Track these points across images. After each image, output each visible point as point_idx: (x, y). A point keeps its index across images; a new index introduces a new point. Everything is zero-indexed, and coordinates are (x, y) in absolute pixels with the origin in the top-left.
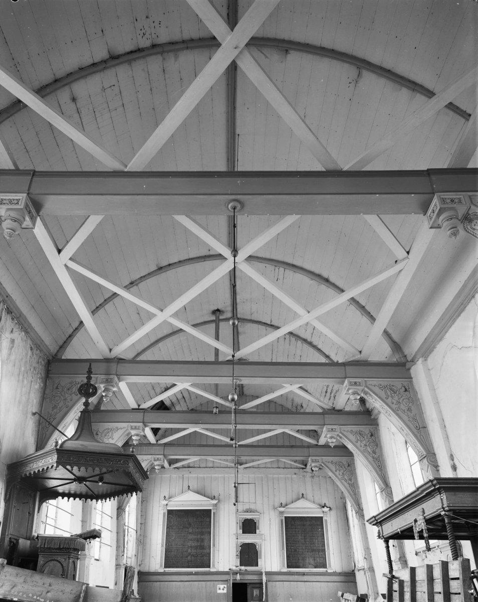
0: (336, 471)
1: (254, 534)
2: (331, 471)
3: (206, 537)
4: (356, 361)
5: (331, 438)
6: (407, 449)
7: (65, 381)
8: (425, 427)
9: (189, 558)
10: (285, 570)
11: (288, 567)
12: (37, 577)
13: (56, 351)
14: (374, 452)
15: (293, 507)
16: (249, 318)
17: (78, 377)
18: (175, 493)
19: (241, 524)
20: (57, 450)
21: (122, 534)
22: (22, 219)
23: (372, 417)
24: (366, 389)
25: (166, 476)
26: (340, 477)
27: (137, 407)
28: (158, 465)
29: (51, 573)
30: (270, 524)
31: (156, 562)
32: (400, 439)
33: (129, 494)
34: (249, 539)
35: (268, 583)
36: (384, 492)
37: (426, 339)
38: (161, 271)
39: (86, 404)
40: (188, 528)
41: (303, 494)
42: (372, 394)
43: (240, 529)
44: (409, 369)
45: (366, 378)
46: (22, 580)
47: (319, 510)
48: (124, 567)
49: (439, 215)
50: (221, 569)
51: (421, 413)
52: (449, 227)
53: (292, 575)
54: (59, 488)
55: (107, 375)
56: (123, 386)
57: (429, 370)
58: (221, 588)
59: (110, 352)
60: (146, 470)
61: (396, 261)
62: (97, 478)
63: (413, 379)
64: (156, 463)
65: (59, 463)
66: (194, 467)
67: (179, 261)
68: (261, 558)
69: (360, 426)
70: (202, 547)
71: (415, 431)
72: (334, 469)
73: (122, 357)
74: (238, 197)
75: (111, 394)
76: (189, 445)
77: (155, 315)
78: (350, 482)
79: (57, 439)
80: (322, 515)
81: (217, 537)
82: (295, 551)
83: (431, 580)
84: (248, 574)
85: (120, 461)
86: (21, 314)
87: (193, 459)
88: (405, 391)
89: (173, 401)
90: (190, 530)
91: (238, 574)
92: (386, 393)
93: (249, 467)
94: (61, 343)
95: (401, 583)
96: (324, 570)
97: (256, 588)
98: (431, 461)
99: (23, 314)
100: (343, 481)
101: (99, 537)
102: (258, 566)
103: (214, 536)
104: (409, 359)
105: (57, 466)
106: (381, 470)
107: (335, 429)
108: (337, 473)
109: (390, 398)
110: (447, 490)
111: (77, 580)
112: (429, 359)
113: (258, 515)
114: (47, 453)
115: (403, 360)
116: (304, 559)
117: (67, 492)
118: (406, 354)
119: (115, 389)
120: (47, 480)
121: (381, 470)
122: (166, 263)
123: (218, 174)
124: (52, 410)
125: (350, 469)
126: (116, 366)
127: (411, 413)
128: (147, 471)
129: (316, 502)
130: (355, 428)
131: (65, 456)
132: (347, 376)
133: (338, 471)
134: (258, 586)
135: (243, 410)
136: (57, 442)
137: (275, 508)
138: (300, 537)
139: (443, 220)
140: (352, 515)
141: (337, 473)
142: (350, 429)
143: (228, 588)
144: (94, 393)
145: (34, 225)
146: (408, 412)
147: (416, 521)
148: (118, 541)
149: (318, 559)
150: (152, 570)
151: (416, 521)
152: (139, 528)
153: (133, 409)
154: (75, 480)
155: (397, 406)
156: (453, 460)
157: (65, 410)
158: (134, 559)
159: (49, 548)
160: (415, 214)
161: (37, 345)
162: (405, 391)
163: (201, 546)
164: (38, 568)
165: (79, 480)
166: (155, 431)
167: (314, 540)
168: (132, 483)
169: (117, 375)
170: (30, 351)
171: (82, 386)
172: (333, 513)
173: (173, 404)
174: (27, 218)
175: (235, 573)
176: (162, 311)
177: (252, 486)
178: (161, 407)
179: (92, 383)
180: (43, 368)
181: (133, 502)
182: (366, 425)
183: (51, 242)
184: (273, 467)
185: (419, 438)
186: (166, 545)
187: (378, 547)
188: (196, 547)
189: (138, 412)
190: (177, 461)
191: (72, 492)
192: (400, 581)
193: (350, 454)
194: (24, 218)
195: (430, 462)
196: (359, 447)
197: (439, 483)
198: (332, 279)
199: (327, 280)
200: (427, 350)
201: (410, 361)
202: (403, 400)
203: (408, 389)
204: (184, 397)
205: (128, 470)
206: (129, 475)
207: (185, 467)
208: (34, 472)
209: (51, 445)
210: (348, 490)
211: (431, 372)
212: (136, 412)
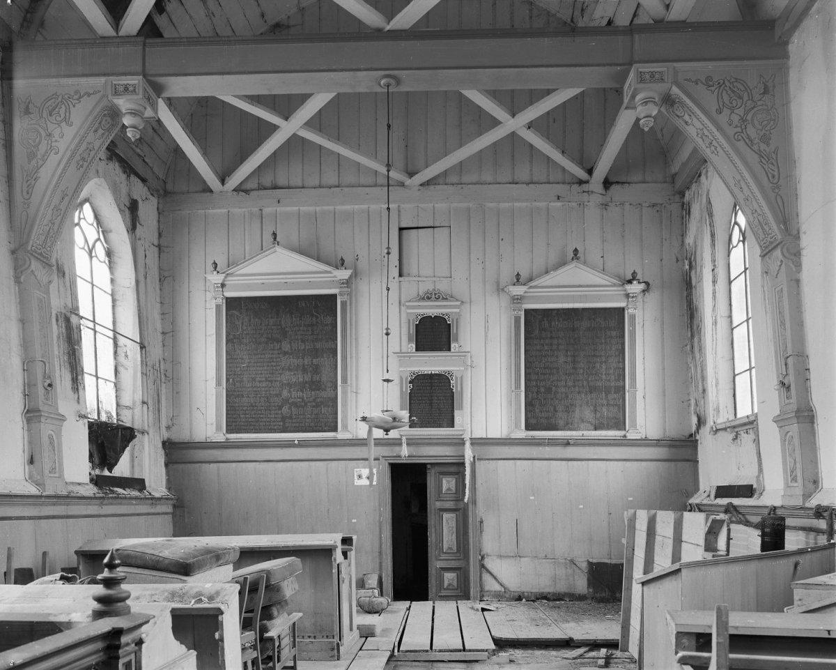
0: (720, 111)
9: (285, 410)
10: (522, 433)
11: (529, 427)
15: (549, 283)
19: (413, 331)
30: (486, 329)
34: (432, 363)
41: (576, 251)
43: (410, 340)
47: (617, 291)
58: (364, 477)
68: (461, 408)
78: (763, 147)
80: (622, 305)
82: (549, 390)
84: (425, 444)
90: (286, 346)
96: (622, 433)
100: (741, 144)
102: (453, 426)
108: (723, 119)
116: (569, 409)
127: (768, 145)
133: (726, 112)
134: (452, 469)
138: (562, 359)
149: (604, 409)
167: (598, 365)
172: (653, 298)
177: (441, 234)
186: (228, 380)
195: (787, 255)
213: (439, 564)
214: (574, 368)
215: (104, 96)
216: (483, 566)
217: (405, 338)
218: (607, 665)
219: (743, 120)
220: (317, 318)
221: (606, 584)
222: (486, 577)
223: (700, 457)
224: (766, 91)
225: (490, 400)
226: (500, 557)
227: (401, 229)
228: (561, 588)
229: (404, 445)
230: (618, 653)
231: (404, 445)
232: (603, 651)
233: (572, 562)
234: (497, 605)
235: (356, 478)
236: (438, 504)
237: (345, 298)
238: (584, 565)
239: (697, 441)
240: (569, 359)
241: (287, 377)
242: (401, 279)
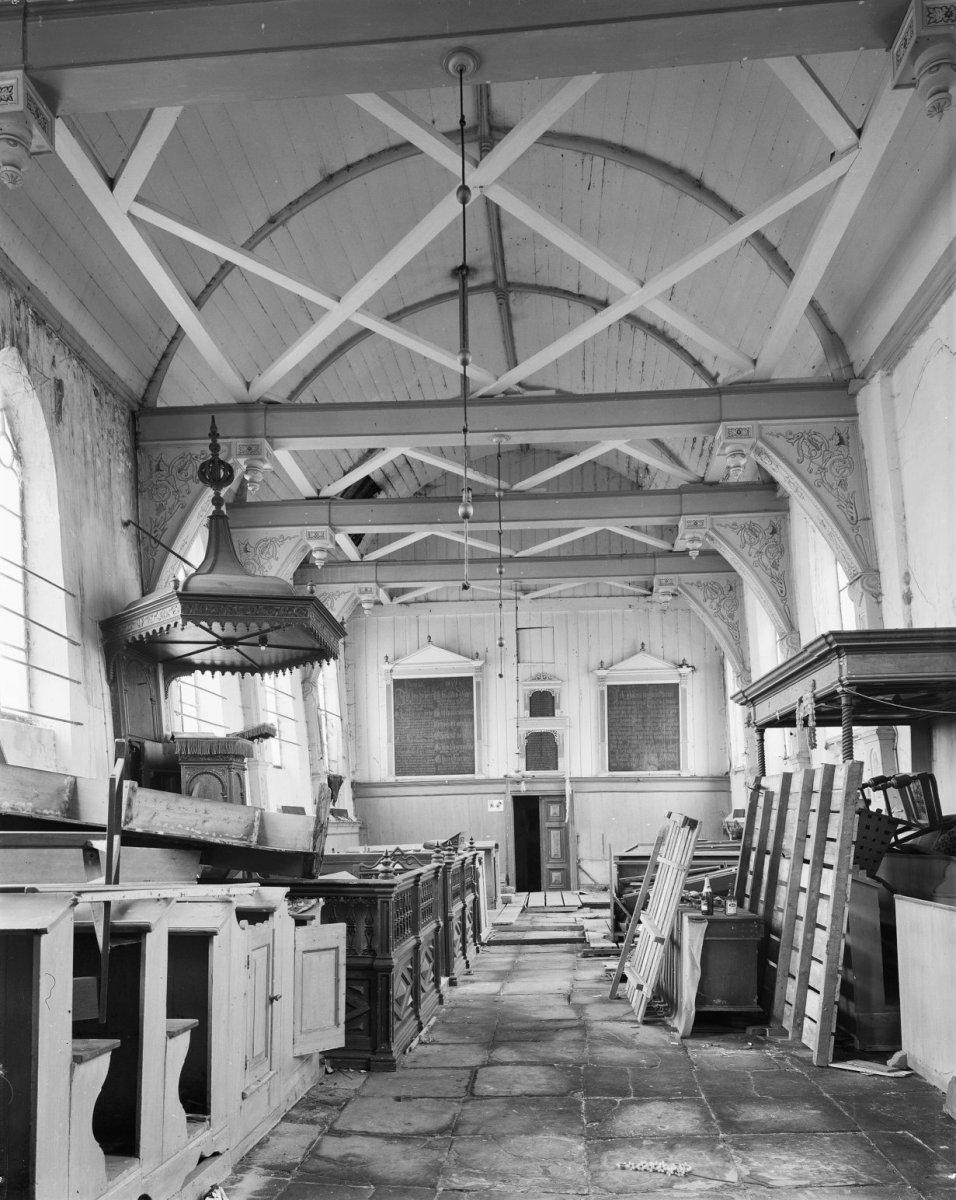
2: (696, 601)
3: (465, 724)
4: (745, 383)
5: (693, 540)
7: (170, 454)
8: (868, 519)
9: (437, 759)
10: (607, 774)
12: (184, 802)
13: (142, 391)
14: (775, 566)
15: (624, 667)
16: (532, 281)
17: (192, 445)
18: (400, 647)
19: (528, 701)
20: (178, 594)
21: (315, 726)
22: (26, 134)
23: (779, 494)
24: (760, 444)
25: (386, 619)
26: (712, 612)
27: (315, 494)
28: (368, 602)
29: (205, 795)
30: (580, 699)
31: (380, 764)
33: (317, 664)
34: (542, 725)
35: (575, 795)
36: (785, 641)
37: (892, 329)
38: (333, 185)
39: (217, 501)
40: (432, 710)
42: (771, 454)
43: (525, 708)
44: (854, 395)
46: (163, 806)
47: (675, 672)
48: (326, 776)
49: (914, 55)
51: (864, 488)
52: (933, 89)
53: (618, 781)
54: (193, 657)
56: (283, 456)
57: (893, 396)
59: (248, 389)
60: (339, 620)
61: (833, 155)
62: (255, 639)
64: (364, 598)
65: (186, 618)
66: (437, 601)
67: (369, 157)
69: (751, 514)
70: (459, 741)
71: (847, 526)
72: (701, 598)
73: (273, 399)
74: (470, 41)
75: (260, 477)
76: (423, 562)
77: (326, 310)
79: (175, 573)
80: (677, 682)
81: (484, 725)
82: (625, 743)
83: (808, 791)
84: (539, 783)
85: (291, 609)
86: (62, 322)
87: (430, 588)
89: (387, 471)
90: (437, 714)
91: (523, 783)
92: (799, 448)
93: (542, 598)
94: (149, 372)
95: (769, 796)
96: (677, 772)
97: (555, 803)
98: (869, 586)
99: (66, 322)
100: (717, 619)
101: (273, 736)
104: (858, 371)
105: (184, 624)
107: (702, 522)
108: (707, 605)
110: (850, 650)
111: (249, 803)
112: (896, 372)
114: (162, 600)
115: (845, 374)
116: (639, 756)
117: (208, 662)
119: (267, 466)
120: (171, 645)
122: (341, 165)
125: (732, 593)
126: (263, 418)
128: (342, 623)
129: (666, 657)
130: (742, 519)
131: (195, 605)
132: (724, 416)
133: (709, 601)
134: (557, 799)
135: (520, 491)
136: (176, 582)
137: (589, 671)
138: (634, 721)
139: (921, 69)
141: (707, 605)
143: (506, 803)
144: (229, 479)
145: (52, 142)
146: (840, 489)
147: (801, 701)
148: (310, 736)
150: (376, 779)
151: (801, 701)
152: (345, 713)
153: (307, 499)
154: (218, 644)
156: (908, 583)
157: (179, 512)
158: (341, 762)
159: (195, 756)
160: (867, 48)
161: (104, 384)
163: (456, 739)
164: (183, 786)
165: (227, 642)
166: (357, 539)
168: (318, 646)
169: (267, 437)
170: (94, 399)
171: (203, 465)
173: (387, 477)
174: (36, 131)
176: (338, 299)
177: (547, 633)
178: (367, 489)
179: (222, 456)
180: (125, 428)
181: (328, 674)
182: (766, 511)
183: (94, 170)
184: (588, 594)
185: (854, 541)
186: (396, 738)
187: (739, 736)
188: (449, 742)
189: (318, 504)
190: (404, 591)
191: (218, 662)
192: (767, 793)
193: (728, 569)
194: (30, 132)
196: (709, 609)
197: (837, 641)
198: (710, 182)
199: (698, 185)
200: (893, 353)
201: (859, 378)
203: (845, 440)
205: (308, 625)
206: (311, 633)
207: (421, 602)
208: (148, 634)
209: (165, 588)
210: (725, 637)
211: (896, 401)
212: (313, 504)
214: (644, 727)
215: (354, 594)
216: (579, 867)
219: (718, 605)
222: (582, 874)
223: (732, 790)
224: (731, 589)
225: (583, 749)
226: (592, 860)
227: (518, 629)
236: (548, 824)
237: (479, 679)
240: (640, 720)
241: (437, 735)
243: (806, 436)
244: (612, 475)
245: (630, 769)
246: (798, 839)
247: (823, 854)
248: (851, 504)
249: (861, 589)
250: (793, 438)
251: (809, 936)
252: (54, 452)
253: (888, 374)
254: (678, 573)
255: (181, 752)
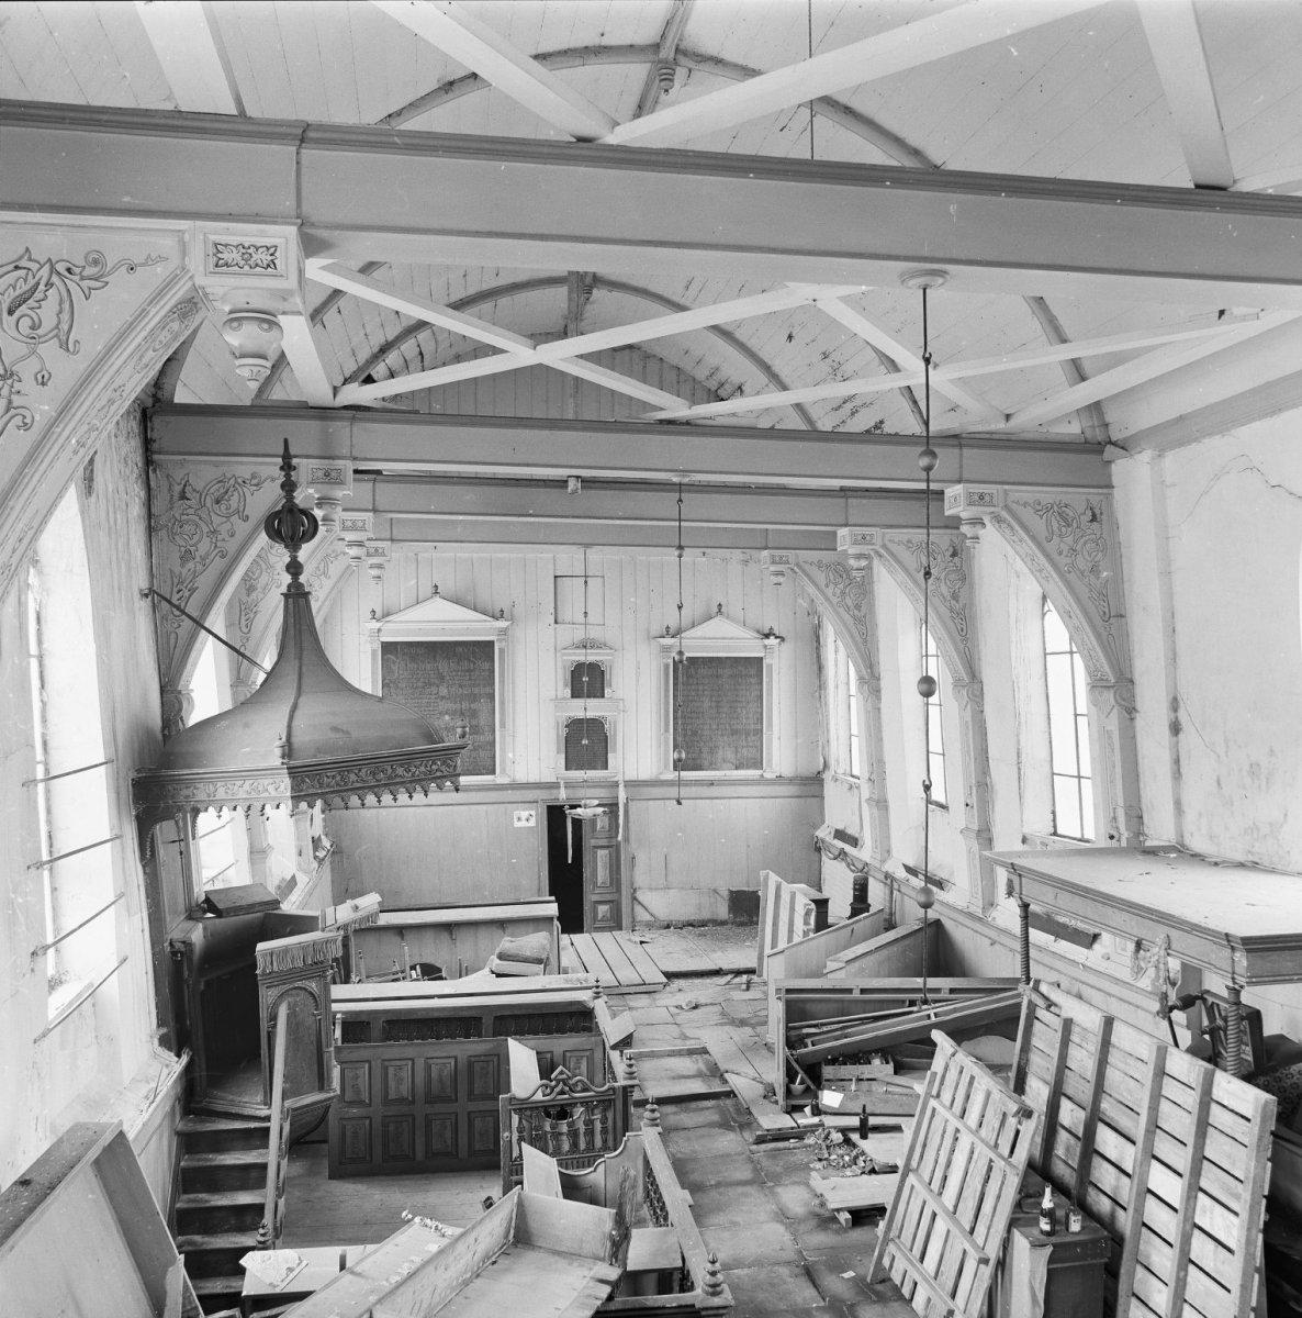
1: (601, 700)
6: (1044, 615)
7: (202, 473)
8: (1122, 616)
10: (671, 775)
14: (955, 597)
17: (242, 463)
30: (638, 675)
32: (1032, 588)
34: (590, 708)
45: (1008, 483)
47: (759, 643)
50: (521, 777)
55: (329, 458)
58: (523, 819)
63: (1115, 491)
68: (615, 751)
71: (1098, 622)
81: (509, 707)
82: (695, 733)
88: (1092, 521)
90: (444, 691)
92: (1048, 523)
96: (759, 772)
100: (841, 610)
102: (606, 768)
103: (502, 703)
106: (965, 639)
108: (829, 591)
109: (1056, 539)
113: (608, 655)
115: (1099, 436)
116: (712, 751)
118: (1108, 419)
121: (965, 639)
123: (896, 175)
124: (182, 566)
126: (348, 429)
129: (748, 621)
138: (707, 704)
140: (836, 661)
141: (829, 591)
142: (906, 538)
155: (1069, 561)
156: (1175, 710)
162: (1092, 521)
175: (554, 786)
202: (1085, 543)
204: (421, 354)
213: (595, 898)
216: (635, 899)
217: (561, 684)
218: (748, 989)
219: (843, 593)
220: (475, 663)
221: (745, 908)
222: (638, 908)
225: (641, 744)
226: (651, 889)
227: (556, 577)
228: (706, 915)
229: (562, 789)
230: (755, 978)
231: (562, 789)
232: (745, 977)
233: (715, 891)
234: (652, 936)
235: (515, 820)
236: (593, 842)
238: (726, 894)
239: (823, 780)
240: (714, 704)
242: (557, 626)
243: (1055, 508)
244: (682, 377)
245: (699, 768)
246: (1147, 1131)
247: (1200, 1175)
248: (1103, 596)
249: (1113, 702)
250: (1042, 510)
251: (1182, 1274)
252: (85, 537)
253: (1160, 456)
254: (795, 549)
255: (264, 970)
